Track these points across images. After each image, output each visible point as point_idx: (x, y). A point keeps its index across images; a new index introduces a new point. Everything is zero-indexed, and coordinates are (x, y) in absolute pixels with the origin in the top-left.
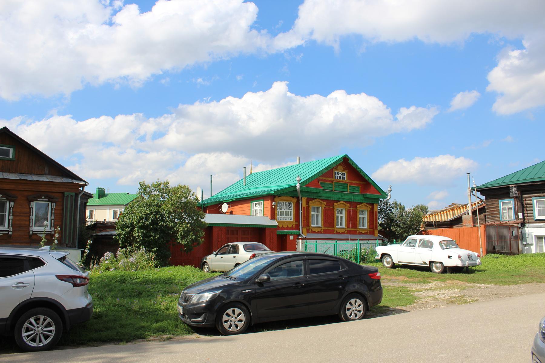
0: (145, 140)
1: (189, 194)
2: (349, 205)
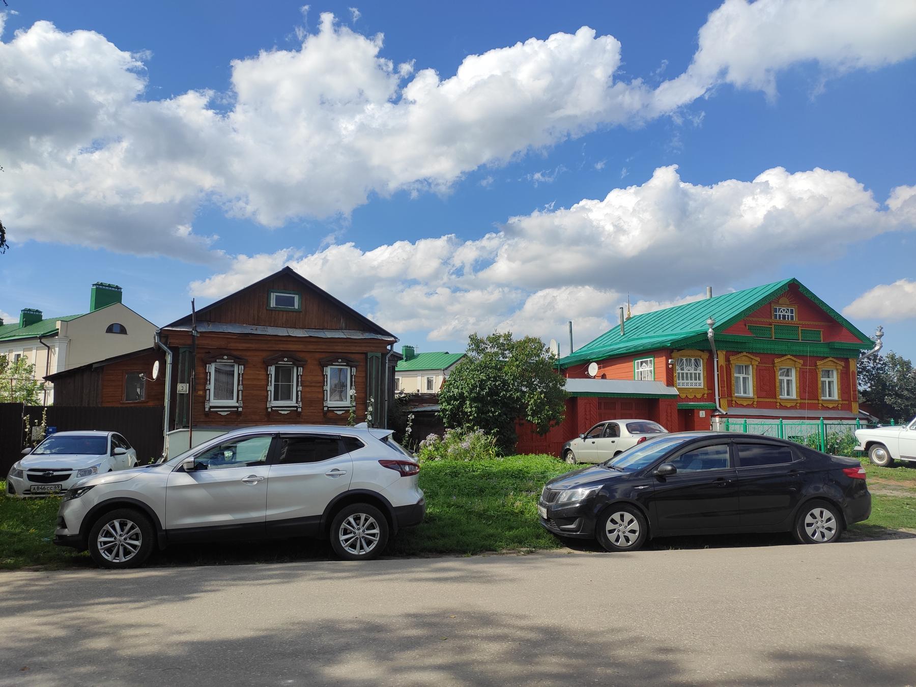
0: (462, 275)
1: (541, 350)
2: (801, 362)
